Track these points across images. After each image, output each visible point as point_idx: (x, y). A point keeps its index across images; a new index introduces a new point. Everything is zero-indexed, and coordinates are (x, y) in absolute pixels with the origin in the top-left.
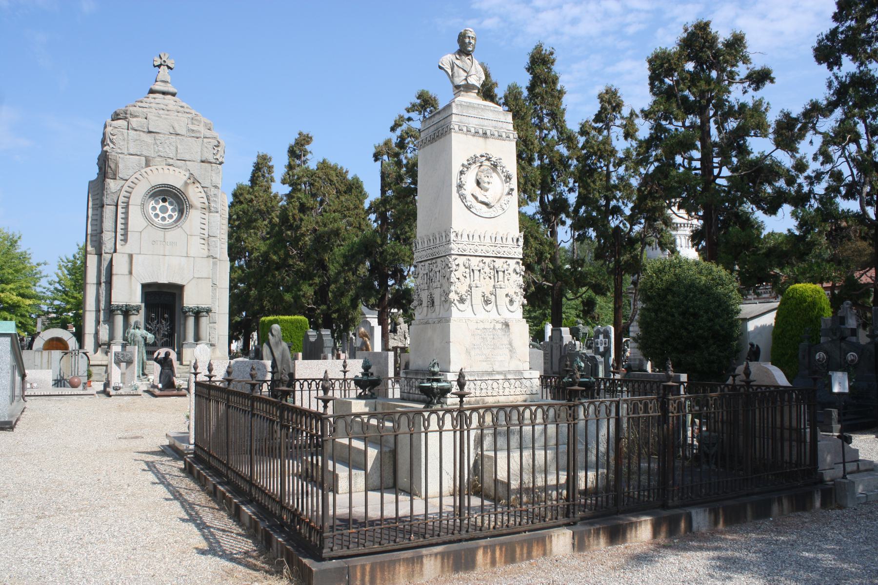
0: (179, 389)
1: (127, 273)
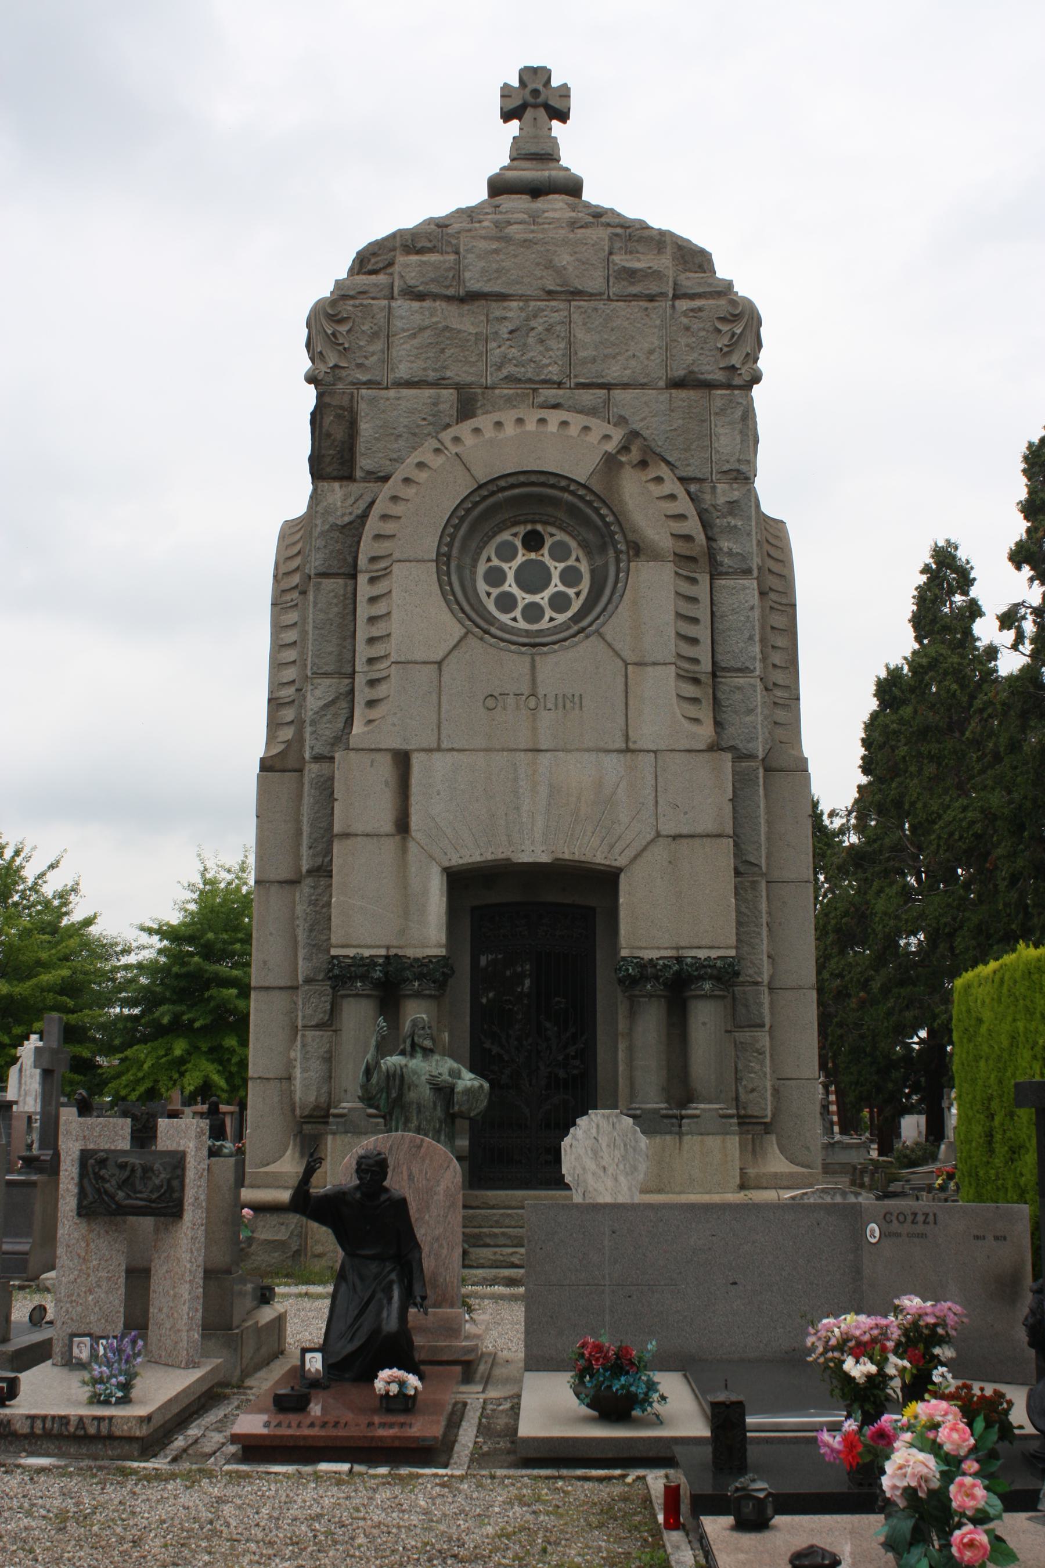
0: (300, 1245)
1: (388, 827)
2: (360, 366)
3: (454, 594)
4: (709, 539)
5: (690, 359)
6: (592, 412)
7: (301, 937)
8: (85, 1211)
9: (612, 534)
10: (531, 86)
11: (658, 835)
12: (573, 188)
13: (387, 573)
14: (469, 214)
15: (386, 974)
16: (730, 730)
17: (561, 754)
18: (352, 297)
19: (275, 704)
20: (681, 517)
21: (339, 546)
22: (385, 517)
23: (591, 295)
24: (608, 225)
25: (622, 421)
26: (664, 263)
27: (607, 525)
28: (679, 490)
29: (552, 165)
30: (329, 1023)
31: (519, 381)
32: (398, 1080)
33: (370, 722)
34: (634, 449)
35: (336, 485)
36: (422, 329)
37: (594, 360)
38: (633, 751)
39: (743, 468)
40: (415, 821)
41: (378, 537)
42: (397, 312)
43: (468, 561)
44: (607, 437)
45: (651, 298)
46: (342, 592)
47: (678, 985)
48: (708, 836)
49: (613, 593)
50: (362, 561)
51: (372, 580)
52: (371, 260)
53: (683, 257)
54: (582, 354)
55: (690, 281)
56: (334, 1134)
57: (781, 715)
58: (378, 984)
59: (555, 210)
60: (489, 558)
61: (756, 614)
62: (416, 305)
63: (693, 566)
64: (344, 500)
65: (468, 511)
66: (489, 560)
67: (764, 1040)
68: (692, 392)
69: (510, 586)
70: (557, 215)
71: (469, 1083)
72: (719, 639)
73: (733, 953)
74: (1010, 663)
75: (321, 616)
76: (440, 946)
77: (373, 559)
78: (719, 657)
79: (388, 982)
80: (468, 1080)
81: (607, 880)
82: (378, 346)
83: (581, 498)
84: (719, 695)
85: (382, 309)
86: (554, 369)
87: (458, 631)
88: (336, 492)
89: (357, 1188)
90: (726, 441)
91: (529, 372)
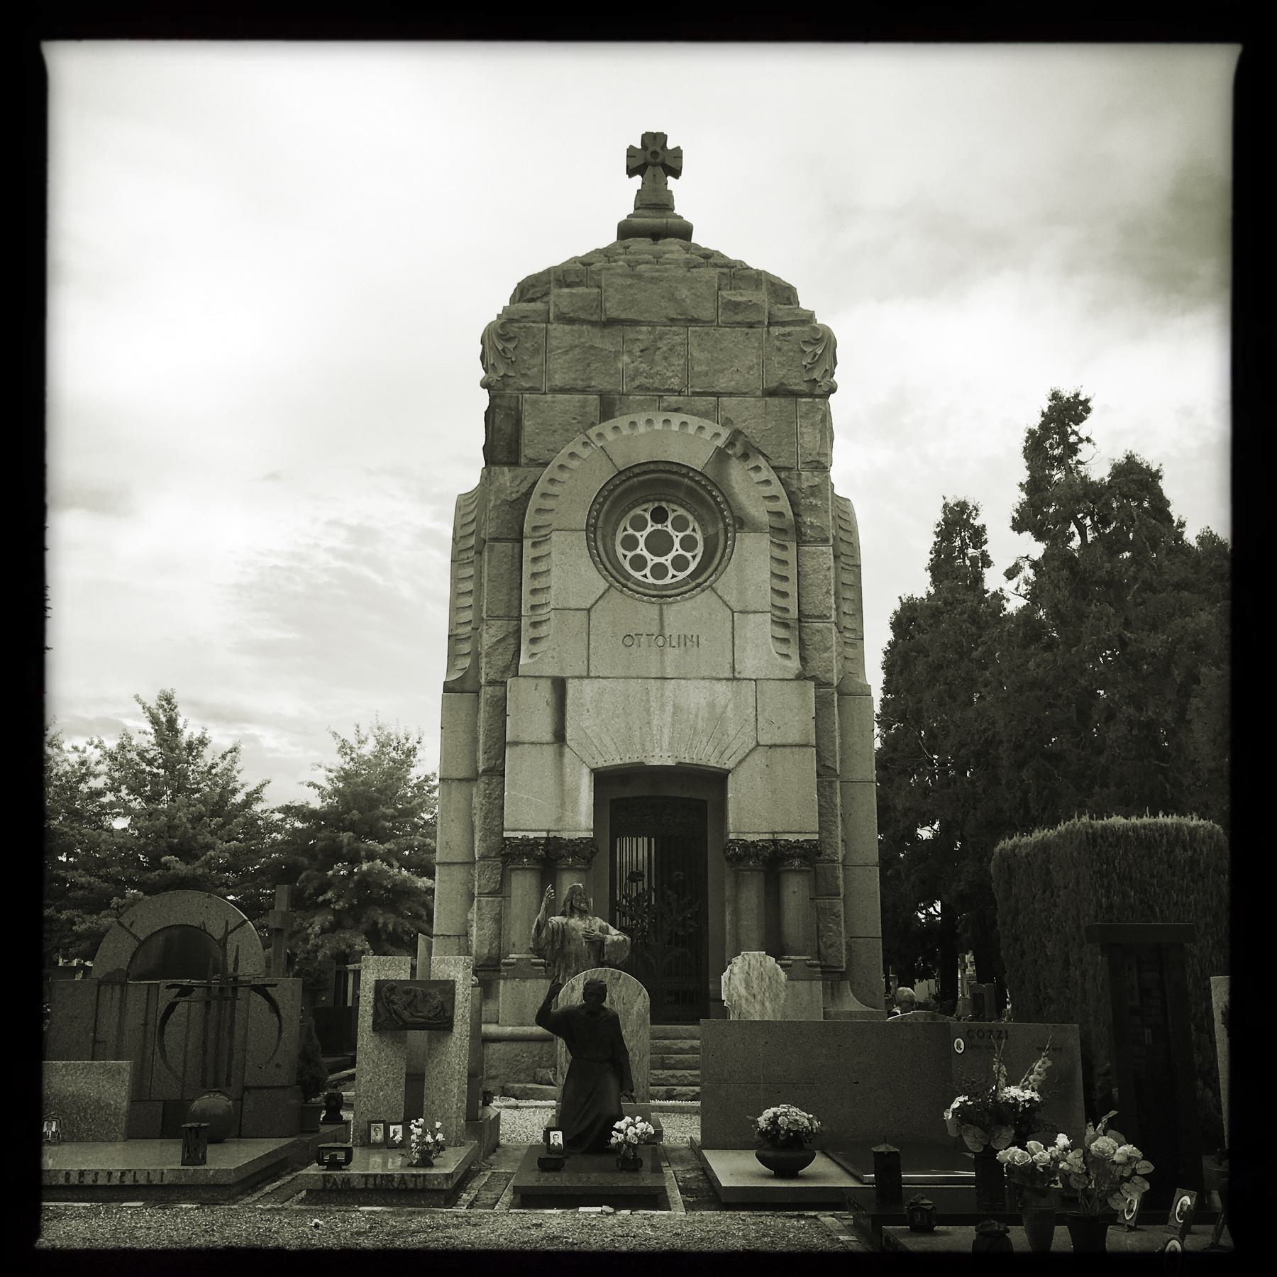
1: (548, 737)
2: (524, 375)
3: (599, 556)
4: (796, 515)
5: (782, 373)
6: (705, 415)
7: (478, 821)
8: (377, 1027)
9: (722, 511)
10: (651, 149)
11: (758, 745)
12: (684, 232)
13: (546, 539)
14: (606, 253)
15: (547, 852)
16: (813, 664)
17: (683, 681)
18: (518, 321)
19: (453, 639)
20: (774, 498)
21: (508, 517)
22: (544, 495)
23: (705, 322)
24: (716, 265)
25: (727, 422)
26: (761, 296)
27: (718, 504)
28: (773, 477)
29: (668, 213)
30: (500, 891)
31: (648, 389)
32: (562, 934)
33: (533, 655)
34: (738, 444)
35: (506, 469)
36: (572, 347)
37: (706, 374)
38: (739, 679)
39: (822, 459)
40: (569, 733)
41: (539, 511)
42: (553, 334)
43: (610, 529)
44: (717, 435)
45: (751, 325)
46: (510, 552)
47: (773, 860)
48: (796, 746)
49: (722, 556)
50: (527, 529)
51: (534, 545)
52: (529, 290)
53: (775, 292)
54: (697, 369)
55: (781, 311)
56: (505, 979)
57: (850, 652)
58: (540, 860)
59: (672, 252)
60: (625, 529)
61: (832, 574)
62: (567, 328)
63: (784, 537)
64: (512, 481)
65: (611, 491)
66: (625, 529)
67: (840, 907)
68: (782, 400)
69: (642, 550)
70: (675, 256)
71: (615, 938)
72: (803, 593)
73: (816, 837)
74: (1015, 604)
75: (495, 571)
76: (588, 830)
77: (535, 528)
78: (803, 607)
79: (547, 857)
80: (614, 935)
81: (717, 779)
82: (538, 360)
83: (698, 482)
84: (803, 636)
85: (540, 330)
86: (676, 380)
87: (603, 585)
88: (505, 476)
89: (582, 1007)
90: (809, 438)
91: (656, 382)
